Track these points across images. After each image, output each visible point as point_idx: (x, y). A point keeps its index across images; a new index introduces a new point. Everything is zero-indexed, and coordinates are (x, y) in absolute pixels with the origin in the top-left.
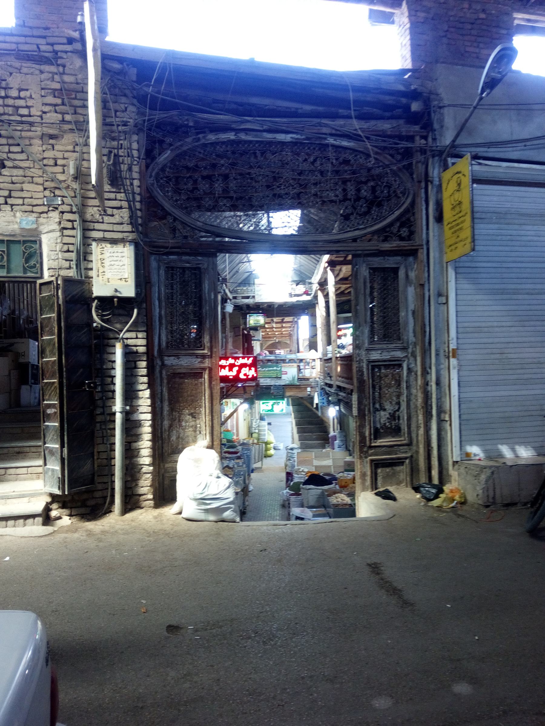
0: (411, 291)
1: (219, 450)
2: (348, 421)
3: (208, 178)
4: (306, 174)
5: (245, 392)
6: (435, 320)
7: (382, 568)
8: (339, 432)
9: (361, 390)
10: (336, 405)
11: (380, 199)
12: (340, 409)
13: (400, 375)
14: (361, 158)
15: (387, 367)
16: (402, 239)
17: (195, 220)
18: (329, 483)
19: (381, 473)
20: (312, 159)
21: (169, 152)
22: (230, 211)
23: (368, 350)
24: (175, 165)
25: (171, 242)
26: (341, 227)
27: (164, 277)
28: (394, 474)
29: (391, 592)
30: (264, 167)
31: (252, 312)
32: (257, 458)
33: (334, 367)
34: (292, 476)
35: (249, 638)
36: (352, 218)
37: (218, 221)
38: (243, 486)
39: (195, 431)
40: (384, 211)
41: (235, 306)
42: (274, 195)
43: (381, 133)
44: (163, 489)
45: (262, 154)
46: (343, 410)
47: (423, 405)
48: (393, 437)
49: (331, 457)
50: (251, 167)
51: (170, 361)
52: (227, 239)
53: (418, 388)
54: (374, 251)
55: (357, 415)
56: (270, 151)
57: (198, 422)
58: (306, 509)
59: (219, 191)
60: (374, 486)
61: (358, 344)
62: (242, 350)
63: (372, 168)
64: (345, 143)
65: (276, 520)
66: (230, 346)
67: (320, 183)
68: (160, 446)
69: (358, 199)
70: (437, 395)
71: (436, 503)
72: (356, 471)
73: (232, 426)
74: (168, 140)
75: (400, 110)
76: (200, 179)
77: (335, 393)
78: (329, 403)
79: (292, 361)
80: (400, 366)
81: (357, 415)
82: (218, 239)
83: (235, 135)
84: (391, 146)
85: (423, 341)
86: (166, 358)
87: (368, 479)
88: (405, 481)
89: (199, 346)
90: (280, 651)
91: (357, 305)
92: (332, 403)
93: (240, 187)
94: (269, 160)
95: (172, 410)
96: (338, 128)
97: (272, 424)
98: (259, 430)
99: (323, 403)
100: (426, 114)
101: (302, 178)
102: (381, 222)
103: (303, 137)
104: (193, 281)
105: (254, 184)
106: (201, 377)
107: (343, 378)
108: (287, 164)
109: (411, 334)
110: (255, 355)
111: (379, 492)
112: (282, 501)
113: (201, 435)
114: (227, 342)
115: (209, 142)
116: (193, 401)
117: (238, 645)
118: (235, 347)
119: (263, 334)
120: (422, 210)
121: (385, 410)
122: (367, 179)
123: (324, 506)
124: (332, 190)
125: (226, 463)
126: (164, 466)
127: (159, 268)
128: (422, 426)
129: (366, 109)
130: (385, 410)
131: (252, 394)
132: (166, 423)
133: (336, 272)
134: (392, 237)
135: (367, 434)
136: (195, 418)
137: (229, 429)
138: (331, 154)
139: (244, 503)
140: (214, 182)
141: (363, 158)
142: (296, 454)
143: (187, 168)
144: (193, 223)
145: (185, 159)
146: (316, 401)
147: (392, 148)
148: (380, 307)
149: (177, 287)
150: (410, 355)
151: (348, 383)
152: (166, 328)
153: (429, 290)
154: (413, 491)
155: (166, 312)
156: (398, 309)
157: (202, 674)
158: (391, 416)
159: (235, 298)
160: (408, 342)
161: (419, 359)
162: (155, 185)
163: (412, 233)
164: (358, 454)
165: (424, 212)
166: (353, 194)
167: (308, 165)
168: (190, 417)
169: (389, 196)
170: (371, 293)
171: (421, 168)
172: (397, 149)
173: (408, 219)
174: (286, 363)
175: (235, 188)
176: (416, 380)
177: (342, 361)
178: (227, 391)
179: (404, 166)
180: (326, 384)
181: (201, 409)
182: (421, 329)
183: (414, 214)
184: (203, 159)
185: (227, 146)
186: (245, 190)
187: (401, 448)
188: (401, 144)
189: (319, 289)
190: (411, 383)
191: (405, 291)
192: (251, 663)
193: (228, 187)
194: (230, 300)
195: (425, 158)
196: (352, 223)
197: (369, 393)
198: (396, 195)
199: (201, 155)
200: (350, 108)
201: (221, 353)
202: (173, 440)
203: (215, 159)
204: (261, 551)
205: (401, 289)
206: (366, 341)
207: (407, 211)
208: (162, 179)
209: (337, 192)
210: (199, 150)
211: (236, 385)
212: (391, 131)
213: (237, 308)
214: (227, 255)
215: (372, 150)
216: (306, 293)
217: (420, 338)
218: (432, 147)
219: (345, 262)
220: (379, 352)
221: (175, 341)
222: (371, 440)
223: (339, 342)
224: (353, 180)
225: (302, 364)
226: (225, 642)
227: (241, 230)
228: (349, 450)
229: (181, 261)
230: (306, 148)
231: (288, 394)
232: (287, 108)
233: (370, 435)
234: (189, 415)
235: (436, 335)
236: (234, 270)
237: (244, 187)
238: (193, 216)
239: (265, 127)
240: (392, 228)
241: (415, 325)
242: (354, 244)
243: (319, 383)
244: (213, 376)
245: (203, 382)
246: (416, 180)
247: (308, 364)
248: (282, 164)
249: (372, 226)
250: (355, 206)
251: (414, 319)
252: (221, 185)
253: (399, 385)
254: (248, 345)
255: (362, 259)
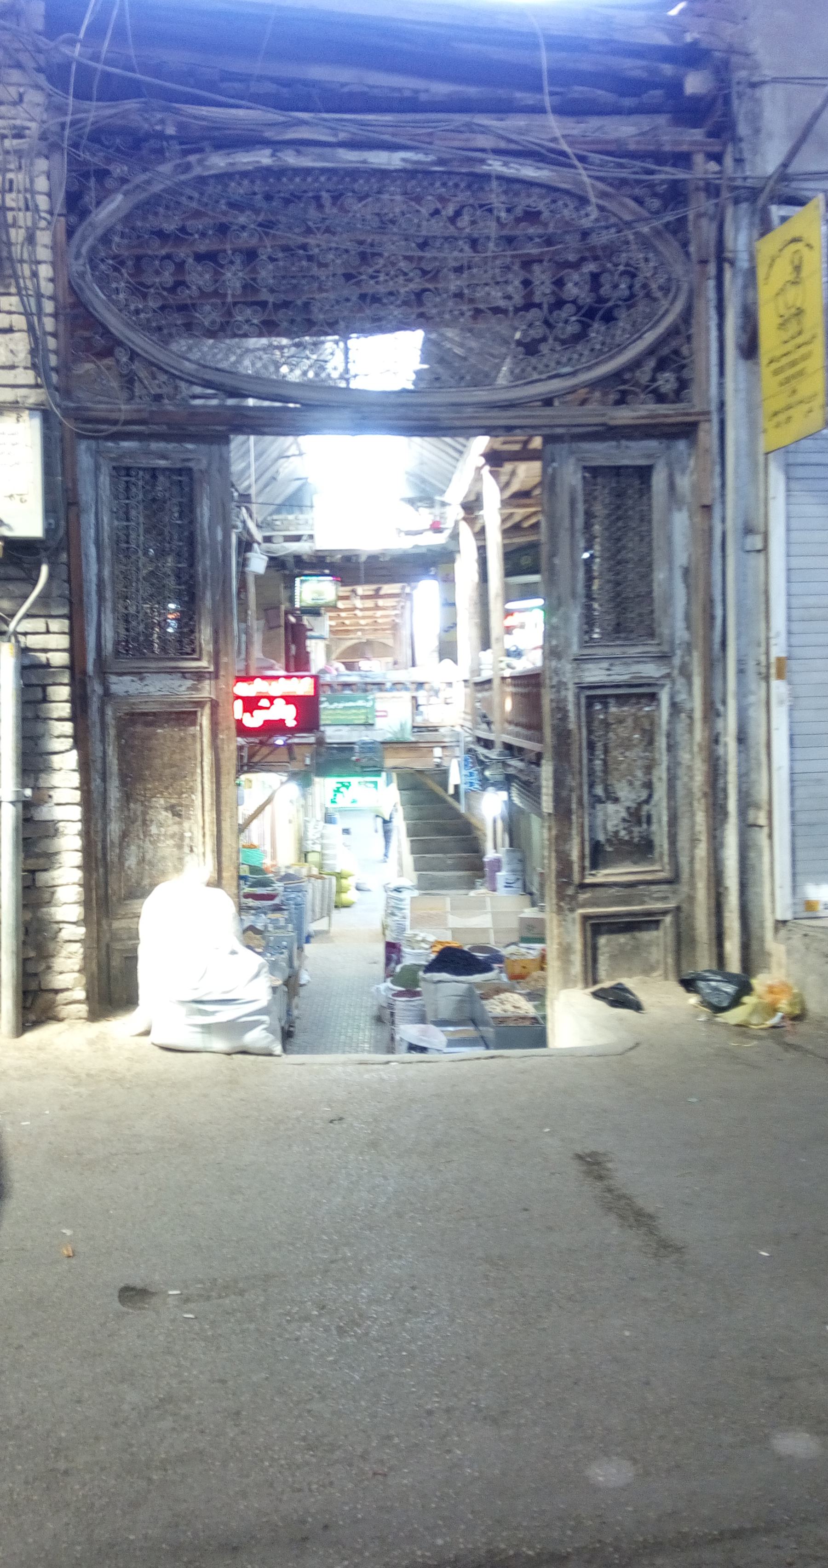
0: (681, 521)
1: (234, 890)
2: (529, 826)
3: (209, 258)
4: (438, 244)
5: (292, 757)
6: (738, 592)
7: (610, 1165)
8: (508, 851)
9: (562, 754)
10: (500, 789)
11: (610, 304)
12: (510, 797)
13: (653, 721)
14: (566, 205)
15: (622, 699)
16: (661, 398)
17: (179, 356)
18: (484, 967)
19: (606, 945)
20: (450, 210)
21: (119, 197)
22: (261, 335)
23: (579, 660)
24: (133, 229)
25: (124, 409)
26: (517, 371)
27: (108, 492)
28: (637, 949)
29: (632, 1219)
30: (339, 229)
31: (307, 572)
32: (317, 909)
33: (496, 700)
34: (400, 951)
35: (307, 1318)
36: (544, 348)
37: (233, 359)
38: (287, 972)
39: (180, 847)
40: (619, 332)
41: (272, 559)
42: (363, 297)
43: (612, 147)
44: (109, 977)
45: (336, 198)
46: (517, 800)
47: (706, 789)
48: (635, 863)
49: (489, 909)
50: (309, 231)
51: (121, 685)
52: (251, 402)
53: (696, 749)
54: (589, 429)
55: (551, 811)
56: (354, 191)
57: (186, 825)
58: (432, 1027)
59: (234, 289)
60: (591, 975)
61: (557, 646)
62: (283, 660)
63: (592, 230)
64: (529, 171)
65: (363, 1051)
66: (257, 652)
67: (469, 268)
68: (102, 880)
69: (559, 304)
70: (739, 765)
71: (734, 1016)
72: (548, 941)
73: (262, 837)
74: (118, 170)
75: (658, 93)
76: (190, 260)
77: (498, 761)
78: (485, 783)
79: (399, 686)
80: (653, 697)
81: (551, 811)
82: (231, 402)
83: (273, 155)
84: (637, 177)
85: (708, 639)
86: (113, 679)
87: (577, 959)
88: (662, 966)
89: (189, 650)
90: (377, 1350)
91: (553, 554)
92: (493, 785)
93: (284, 277)
94: (350, 215)
95: (128, 797)
96: (514, 137)
97: (352, 831)
98: (323, 846)
99: (471, 784)
100: (720, 101)
101: (428, 254)
102: (611, 358)
103: (431, 158)
104: (175, 501)
105: (315, 271)
106: (193, 723)
107: (517, 725)
108: (393, 222)
109: (680, 624)
110: (314, 671)
111: (602, 990)
112: (375, 1008)
113: (193, 855)
114: (249, 643)
115: (212, 172)
116: (174, 778)
117: (280, 1336)
118: (269, 653)
119: (333, 623)
120: (708, 329)
121: (616, 800)
122: (578, 256)
123: (474, 1022)
124: (498, 283)
125: (249, 919)
126: (110, 926)
127: (97, 468)
128: (704, 837)
129: (578, 91)
130: (616, 800)
131: (308, 761)
132: (115, 828)
133: (504, 479)
134: (636, 394)
135: (575, 855)
136: (179, 816)
137: (255, 842)
138: (495, 197)
139: (289, 1012)
140: (222, 266)
141: (572, 206)
142: (408, 901)
143: (160, 234)
144: (172, 363)
145: (156, 214)
146: (455, 778)
147: (638, 182)
148: (608, 559)
149: (138, 515)
150: (676, 672)
151: (530, 739)
152: (114, 610)
153: (723, 520)
154: (681, 990)
155: (112, 573)
156: (650, 566)
157: (201, 1399)
158: (630, 814)
159: (268, 539)
160: (672, 643)
161: (697, 682)
162: (89, 277)
163: (683, 385)
164: (554, 901)
165: (714, 334)
166: (548, 291)
167: (441, 224)
168: (170, 815)
169: (632, 296)
170: (588, 526)
171: (708, 229)
172: (651, 186)
173: (676, 352)
174: (386, 691)
175: (271, 281)
176: (691, 731)
177: (515, 685)
178: (251, 756)
179: (667, 225)
180: (479, 740)
181: (193, 797)
182: (704, 611)
183: (689, 338)
184: (197, 214)
185: (252, 182)
186: (295, 287)
187: (654, 888)
188: (660, 172)
189: (464, 519)
190: (679, 739)
191: (667, 522)
192: (312, 1375)
193: (254, 280)
194: (259, 544)
195: (717, 205)
196: (545, 361)
197: (580, 761)
198: (648, 295)
199: (194, 205)
200: (539, 89)
201: (239, 667)
202: (129, 868)
203: (224, 213)
204: (331, 1122)
205: (657, 516)
206: (575, 640)
207: (673, 332)
208: (102, 261)
209: (510, 289)
210: (188, 191)
211: (271, 741)
212: (638, 143)
213: (276, 563)
214: (252, 438)
215: (593, 186)
216: (436, 528)
217: (701, 633)
218: (732, 179)
219: (525, 455)
220: (605, 665)
221: (136, 639)
222: (583, 868)
223: (510, 642)
224: (546, 258)
225: (422, 695)
226: (252, 1326)
227: (283, 382)
228: (531, 894)
229: (148, 453)
230: (438, 184)
231: (389, 762)
232: (393, 89)
233: (582, 857)
234: (166, 809)
235: (739, 624)
236: (267, 475)
237: (293, 277)
238: (174, 347)
239: (342, 136)
240: (638, 373)
241: (689, 603)
242: (548, 411)
243: (462, 739)
244: (220, 720)
245: (198, 734)
246: (694, 257)
247: (436, 692)
248: (382, 222)
249: (590, 368)
250: (551, 321)
251: (688, 586)
252: (240, 274)
253: (651, 742)
254: (298, 649)
255: (566, 446)
